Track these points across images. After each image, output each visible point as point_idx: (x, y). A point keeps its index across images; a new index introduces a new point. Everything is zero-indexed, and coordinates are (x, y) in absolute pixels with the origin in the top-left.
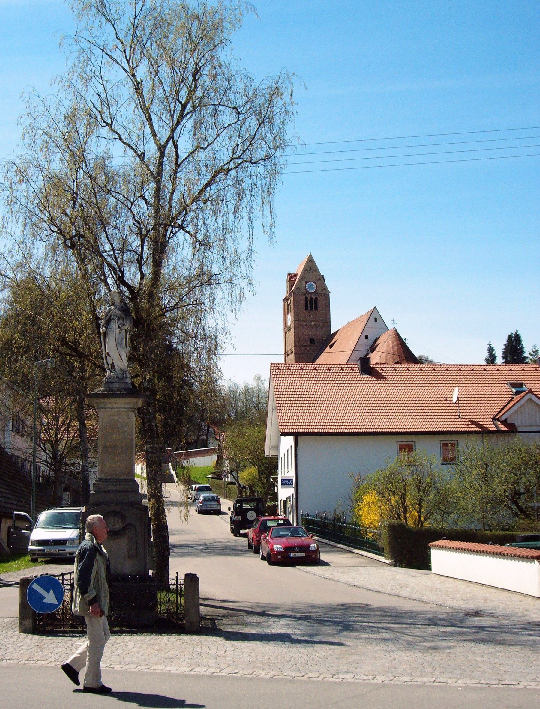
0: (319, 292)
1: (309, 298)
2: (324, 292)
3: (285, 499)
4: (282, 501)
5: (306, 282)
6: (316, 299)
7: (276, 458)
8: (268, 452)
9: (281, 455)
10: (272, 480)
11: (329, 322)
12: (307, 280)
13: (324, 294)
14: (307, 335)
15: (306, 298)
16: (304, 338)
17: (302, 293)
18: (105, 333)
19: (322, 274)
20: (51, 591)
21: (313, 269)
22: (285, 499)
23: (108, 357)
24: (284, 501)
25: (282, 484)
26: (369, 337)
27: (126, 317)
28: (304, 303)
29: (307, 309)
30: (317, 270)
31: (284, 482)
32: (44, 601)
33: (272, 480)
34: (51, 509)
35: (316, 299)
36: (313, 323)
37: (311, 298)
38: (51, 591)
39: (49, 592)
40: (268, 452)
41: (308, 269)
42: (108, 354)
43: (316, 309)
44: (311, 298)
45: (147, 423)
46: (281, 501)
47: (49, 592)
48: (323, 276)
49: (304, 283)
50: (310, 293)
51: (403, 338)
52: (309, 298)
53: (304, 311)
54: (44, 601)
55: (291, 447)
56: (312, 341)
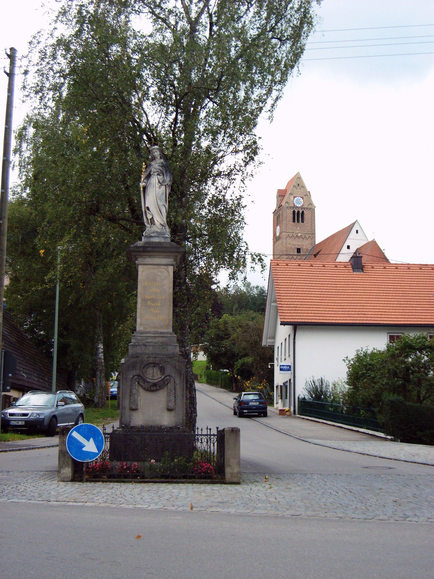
0: (306, 206)
1: (296, 211)
2: (310, 206)
3: (282, 384)
4: (279, 387)
5: (294, 197)
6: (303, 212)
7: (271, 348)
8: (265, 342)
9: (278, 344)
10: (269, 367)
11: (313, 234)
12: (294, 195)
13: (310, 209)
14: (294, 245)
15: (294, 212)
16: (292, 248)
17: (290, 207)
18: (145, 188)
19: (308, 190)
20: (91, 439)
21: (300, 186)
22: (282, 384)
23: (147, 211)
24: (281, 386)
25: (281, 370)
26: (351, 247)
27: (166, 173)
28: (292, 216)
29: (294, 221)
30: (304, 187)
31: (282, 367)
32: (83, 449)
33: (269, 367)
34: (155, 256)
35: (303, 212)
36: (299, 235)
37: (298, 212)
38: (91, 439)
39: (88, 440)
40: (265, 342)
41: (296, 185)
42: (148, 208)
43: (303, 221)
44: (298, 212)
45: (177, 286)
46: (277, 387)
47: (88, 440)
48: (309, 192)
49: (292, 197)
50: (297, 207)
51: (382, 249)
52: (296, 211)
53: (292, 223)
54: (83, 449)
55: (285, 339)
56: (299, 250)
